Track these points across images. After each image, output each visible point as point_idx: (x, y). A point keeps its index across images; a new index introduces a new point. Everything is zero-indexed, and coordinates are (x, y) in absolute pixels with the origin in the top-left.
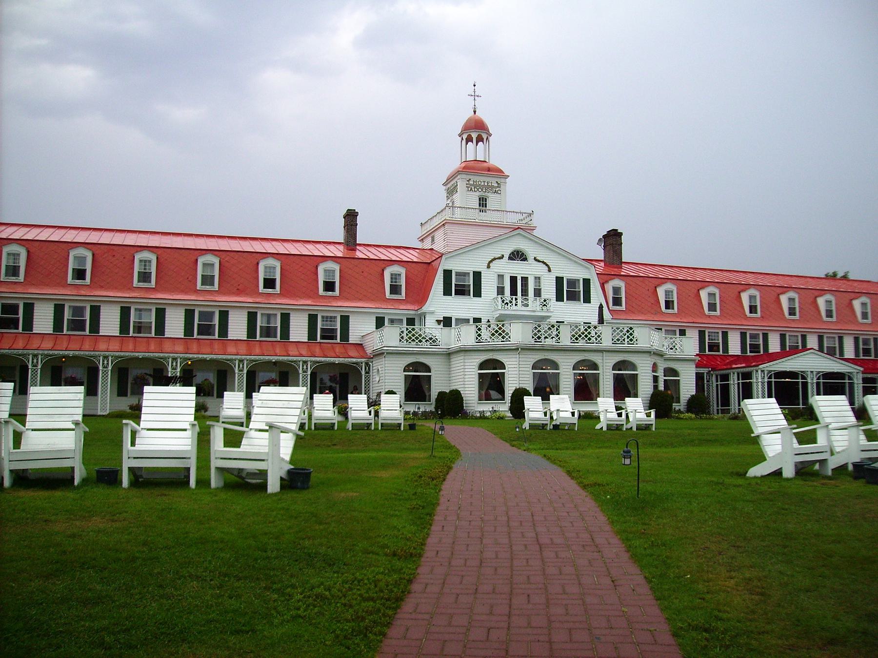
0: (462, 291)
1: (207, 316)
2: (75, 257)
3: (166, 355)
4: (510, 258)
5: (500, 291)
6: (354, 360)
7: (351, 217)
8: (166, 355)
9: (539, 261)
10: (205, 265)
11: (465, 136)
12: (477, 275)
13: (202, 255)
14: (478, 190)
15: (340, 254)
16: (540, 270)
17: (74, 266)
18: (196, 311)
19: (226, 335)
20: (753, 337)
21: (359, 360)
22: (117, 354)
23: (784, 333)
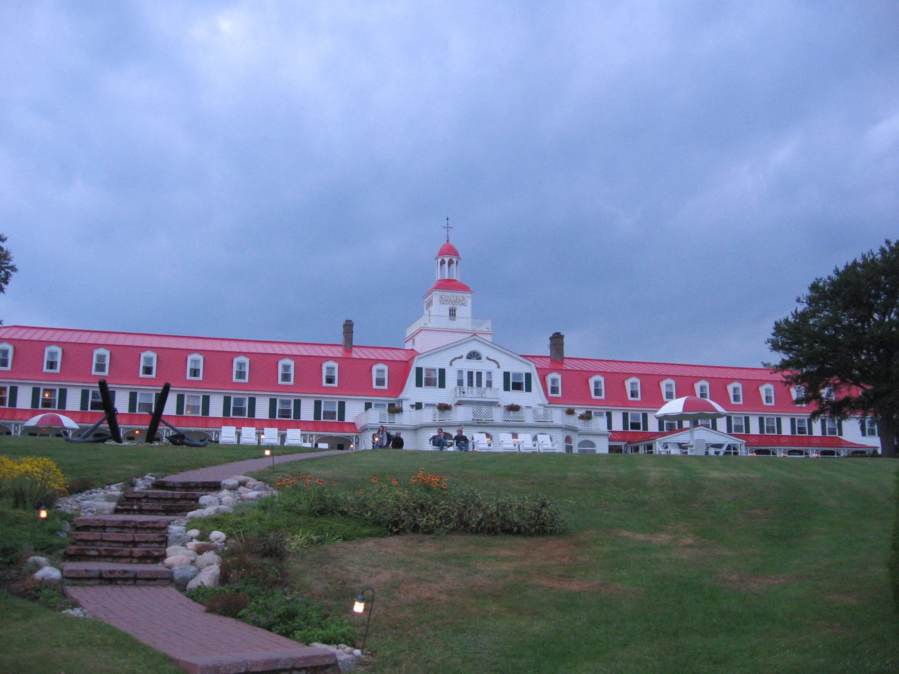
0: (430, 383)
1: (239, 401)
2: (145, 358)
3: (211, 429)
4: (468, 358)
5: (460, 383)
6: (347, 434)
7: (348, 327)
8: (211, 429)
9: (490, 360)
10: (378, 371)
11: (439, 260)
12: (442, 372)
13: (237, 356)
14: (448, 303)
15: (340, 355)
16: (491, 366)
17: (237, 369)
18: (138, 393)
19: (647, 429)
20: (800, 421)
21: (351, 434)
22: (126, 426)
23: (135, 391)
